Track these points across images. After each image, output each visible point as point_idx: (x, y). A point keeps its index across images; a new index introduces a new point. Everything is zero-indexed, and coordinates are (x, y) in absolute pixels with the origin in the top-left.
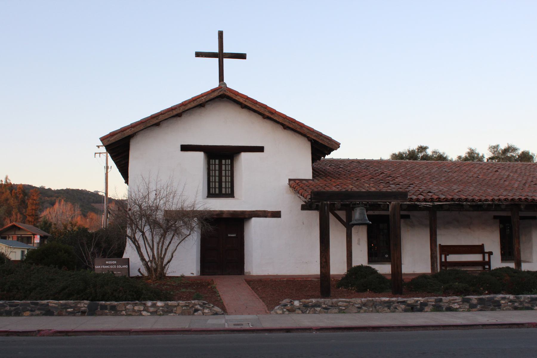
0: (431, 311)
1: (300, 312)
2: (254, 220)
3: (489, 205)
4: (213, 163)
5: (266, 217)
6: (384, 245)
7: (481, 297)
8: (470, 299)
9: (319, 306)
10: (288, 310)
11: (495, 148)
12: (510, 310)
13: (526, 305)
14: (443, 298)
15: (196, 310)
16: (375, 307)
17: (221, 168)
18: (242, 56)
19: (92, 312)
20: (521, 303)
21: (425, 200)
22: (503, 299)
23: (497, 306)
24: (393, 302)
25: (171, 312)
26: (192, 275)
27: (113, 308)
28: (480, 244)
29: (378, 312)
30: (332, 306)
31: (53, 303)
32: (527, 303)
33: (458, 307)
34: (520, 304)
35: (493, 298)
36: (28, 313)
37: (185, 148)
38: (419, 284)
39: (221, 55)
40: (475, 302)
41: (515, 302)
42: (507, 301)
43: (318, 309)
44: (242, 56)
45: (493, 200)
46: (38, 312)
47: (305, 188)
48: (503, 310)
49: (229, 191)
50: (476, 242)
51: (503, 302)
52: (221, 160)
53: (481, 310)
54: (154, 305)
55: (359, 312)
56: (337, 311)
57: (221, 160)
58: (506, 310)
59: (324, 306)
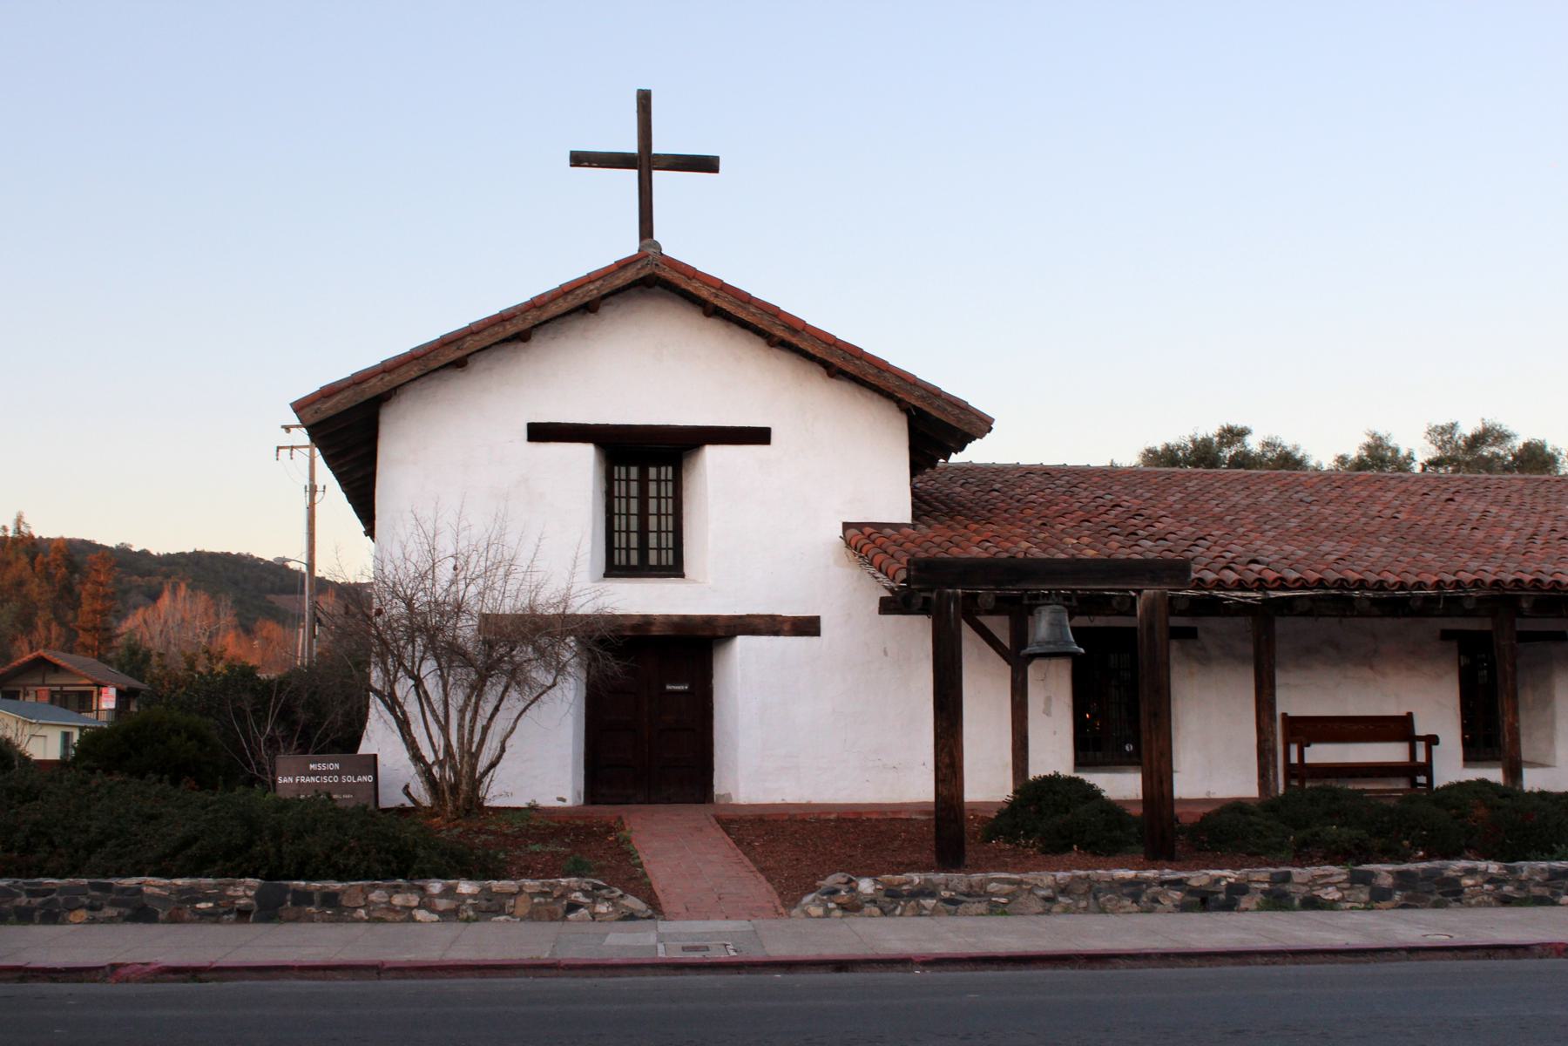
0: (1260, 908)
1: (876, 910)
2: (741, 642)
3: (1427, 598)
4: (623, 476)
5: (776, 633)
6: (1123, 717)
7: (1404, 867)
8: (1372, 874)
9: (932, 895)
10: (843, 907)
11: (1444, 433)
12: (1489, 905)
13: (1537, 891)
14: (1295, 871)
15: (574, 907)
16: (1095, 898)
17: (647, 491)
18: (707, 164)
19: (267, 911)
20: (1522, 885)
21: (1241, 585)
22: (1470, 872)
23: (1450, 893)
24: (1148, 882)
25: (500, 911)
26: (560, 804)
27: (330, 899)
28: (1403, 712)
29: (1103, 910)
30: (968, 895)
31: (153, 885)
32: (1538, 884)
33: (1337, 896)
34: (1518, 889)
35: (1438, 871)
36: (83, 914)
37: (540, 433)
38: (1224, 831)
39: (644, 162)
40: (1386, 881)
41: (1505, 882)
42: (1479, 879)
43: (929, 903)
44: (707, 164)
45: (1439, 584)
46: (110, 912)
47: (890, 551)
48: (1470, 906)
49: (668, 558)
50: (1391, 708)
51: (1468, 882)
52: (646, 466)
53: (1404, 906)
54: (449, 892)
55: (1048, 912)
56: (983, 907)
57: (646, 466)
58: (1479, 905)
59: (945, 894)
